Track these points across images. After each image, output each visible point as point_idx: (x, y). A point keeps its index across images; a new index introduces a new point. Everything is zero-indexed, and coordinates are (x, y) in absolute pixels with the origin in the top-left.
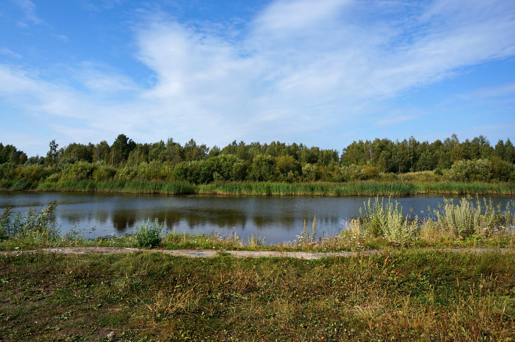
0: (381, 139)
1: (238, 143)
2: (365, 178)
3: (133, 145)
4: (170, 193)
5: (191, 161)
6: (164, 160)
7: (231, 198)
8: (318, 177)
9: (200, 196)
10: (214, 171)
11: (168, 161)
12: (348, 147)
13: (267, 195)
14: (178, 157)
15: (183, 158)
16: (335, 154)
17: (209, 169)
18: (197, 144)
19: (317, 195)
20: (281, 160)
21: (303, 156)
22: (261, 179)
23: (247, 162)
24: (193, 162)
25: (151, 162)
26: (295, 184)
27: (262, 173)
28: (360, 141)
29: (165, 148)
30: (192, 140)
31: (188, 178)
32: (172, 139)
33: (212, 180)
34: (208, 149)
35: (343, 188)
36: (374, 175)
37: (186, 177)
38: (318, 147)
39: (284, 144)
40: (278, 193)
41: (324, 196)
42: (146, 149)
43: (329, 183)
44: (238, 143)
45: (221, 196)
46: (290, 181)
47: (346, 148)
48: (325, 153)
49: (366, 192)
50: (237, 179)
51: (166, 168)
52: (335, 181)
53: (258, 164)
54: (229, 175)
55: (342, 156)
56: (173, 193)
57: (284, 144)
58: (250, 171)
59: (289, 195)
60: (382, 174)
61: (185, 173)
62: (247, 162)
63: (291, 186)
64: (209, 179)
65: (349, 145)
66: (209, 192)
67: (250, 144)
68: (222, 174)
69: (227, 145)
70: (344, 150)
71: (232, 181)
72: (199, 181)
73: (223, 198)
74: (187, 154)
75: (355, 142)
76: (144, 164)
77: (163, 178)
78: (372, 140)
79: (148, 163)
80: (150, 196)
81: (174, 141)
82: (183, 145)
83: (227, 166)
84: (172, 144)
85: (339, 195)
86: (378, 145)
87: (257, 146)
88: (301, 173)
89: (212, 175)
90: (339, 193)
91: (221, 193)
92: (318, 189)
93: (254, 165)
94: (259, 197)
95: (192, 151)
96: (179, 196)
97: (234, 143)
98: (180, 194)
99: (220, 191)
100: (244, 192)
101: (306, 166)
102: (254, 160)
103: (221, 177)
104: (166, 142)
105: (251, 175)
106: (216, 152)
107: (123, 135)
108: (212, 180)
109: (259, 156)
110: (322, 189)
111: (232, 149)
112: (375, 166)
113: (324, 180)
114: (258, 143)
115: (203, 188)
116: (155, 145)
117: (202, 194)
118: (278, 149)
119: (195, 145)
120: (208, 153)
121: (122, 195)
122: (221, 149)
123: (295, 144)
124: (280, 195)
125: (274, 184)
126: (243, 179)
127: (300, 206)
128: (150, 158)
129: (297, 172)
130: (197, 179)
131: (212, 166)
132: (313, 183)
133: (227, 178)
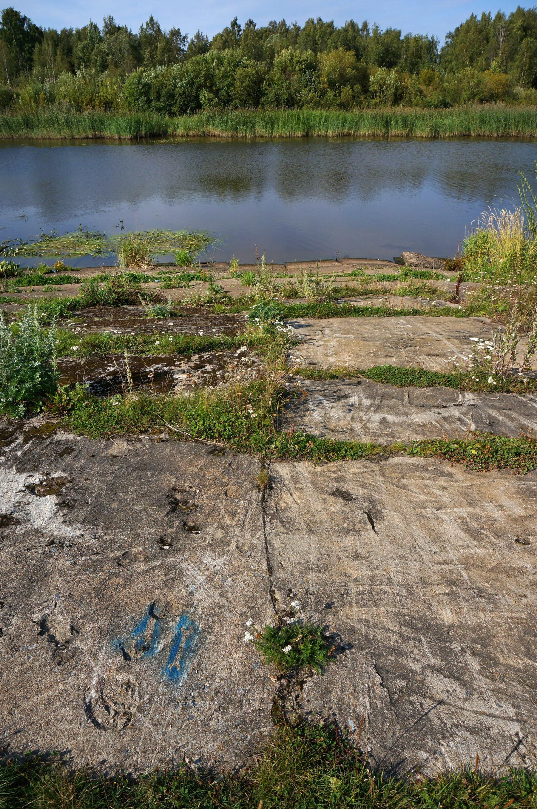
0: (526, 9)
1: (242, 23)
2: (492, 97)
3: (36, 35)
4: (123, 136)
5: (155, 66)
6: (104, 67)
7: (236, 144)
8: (398, 98)
9: (180, 139)
10: (200, 86)
11: (112, 67)
12: (457, 30)
13: (304, 136)
14: (129, 59)
15: (139, 60)
16: (431, 45)
17: (191, 83)
18: (162, 28)
19: (396, 136)
20: (329, 61)
21: (373, 50)
22: (291, 103)
23: (262, 66)
24: (159, 68)
25: (79, 73)
26: (356, 111)
27: (293, 90)
28: (484, 15)
29: (101, 40)
30: (152, 19)
31: (154, 103)
32: (111, 19)
33: (199, 106)
34: (185, 37)
35: (446, 121)
36: (505, 94)
37: (149, 101)
38: (398, 29)
39: (332, 23)
40: (322, 133)
41: (408, 137)
42: (64, 42)
43: (418, 109)
44: (242, 23)
45: (218, 139)
46: (343, 106)
47: (453, 31)
48: (412, 44)
49: (486, 130)
50: (244, 104)
51: (108, 83)
52: (428, 105)
53: (284, 70)
54: (229, 96)
55: (443, 50)
56: (129, 137)
57: (332, 23)
58: (269, 85)
59: (343, 136)
60: (519, 90)
61: (147, 93)
62: (262, 66)
63: (348, 115)
64: (192, 105)
65: (458, 25)
66: (194, 133)
67: (266, 25)
68: (216, 94)
69: (220, 31)
70: (449, 36)
71: (236, 107)
72: (174, 109)
73: (228, 144)
74: (146, 53)
75: (473, 17)
76: (65, 76)
77: (108, 104)
78: (508, 11)
79: (74, 73)
80: (87, 144)
81: (118, 22)
82: (136, 31)
83: (226, 75)
84: (113, 29)
85: (435, 137)
86: (520, 23)
87: (279, 29)
88: (365, 90)
89: (197, 97)
90: (436, 131)
91: (217, 133)
92: (396, 122)
93: (276, 71)
94: (288, 142)
95: (153, 45)
96: (142, 143)
97: (235, 24)
98: (141, 137)
99: (214, 130)
100: (260, 130)
101: (377, 75)
102: (276, 60)
103: (216, 100)
104: (101, 26)
105: (272, 95)
106: (201, 46)
107: (7, 10)
108: (199, 106)
109: (285, 53)
110: (405, 122)
111: (230, 37)
112: (505, 72)
113: (410, 103)
114: (283, 24)
115: (183, 125)
116: (81, 34)
117: (183, 136)
118: (319, 35)
119: (159, 30)
120: (186, 48)
121: (31, 142)
122: (211, 39)
123: (352, 24)
124: (326, 136)
125: (317, 113)
126: (256, 103)
127: (365, 157)
128: (76, 63)
129: (358, 87)
130: (171, 105)
131: (197, 75)
132: (388, 110)
133: (226, 102)
